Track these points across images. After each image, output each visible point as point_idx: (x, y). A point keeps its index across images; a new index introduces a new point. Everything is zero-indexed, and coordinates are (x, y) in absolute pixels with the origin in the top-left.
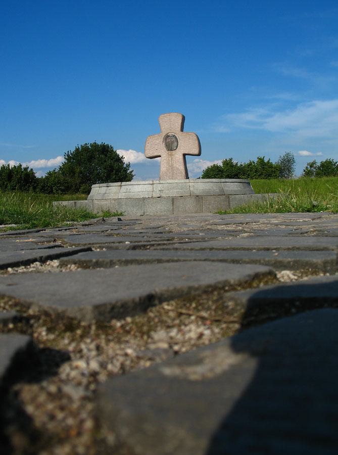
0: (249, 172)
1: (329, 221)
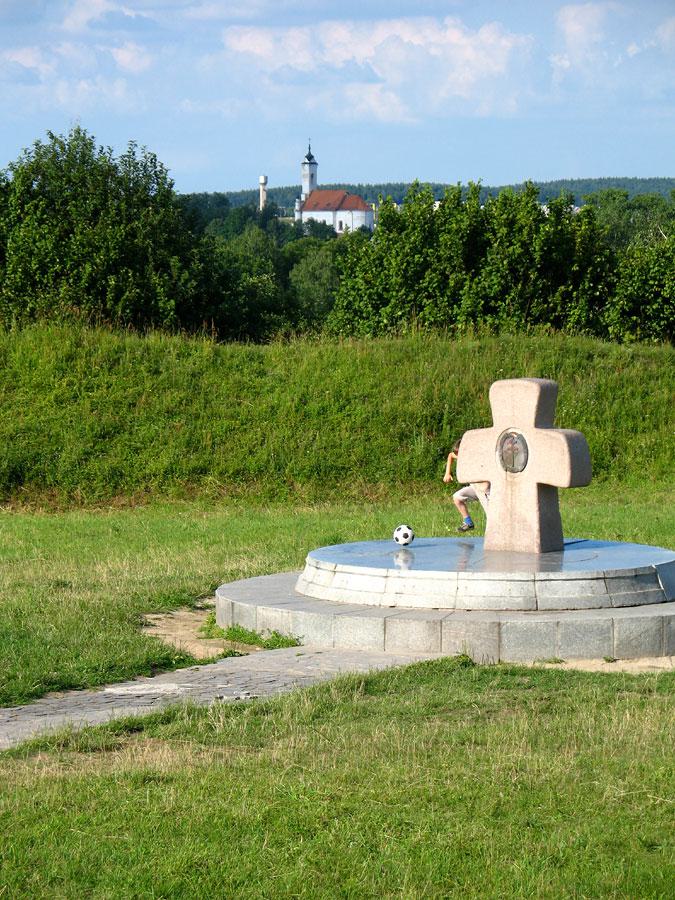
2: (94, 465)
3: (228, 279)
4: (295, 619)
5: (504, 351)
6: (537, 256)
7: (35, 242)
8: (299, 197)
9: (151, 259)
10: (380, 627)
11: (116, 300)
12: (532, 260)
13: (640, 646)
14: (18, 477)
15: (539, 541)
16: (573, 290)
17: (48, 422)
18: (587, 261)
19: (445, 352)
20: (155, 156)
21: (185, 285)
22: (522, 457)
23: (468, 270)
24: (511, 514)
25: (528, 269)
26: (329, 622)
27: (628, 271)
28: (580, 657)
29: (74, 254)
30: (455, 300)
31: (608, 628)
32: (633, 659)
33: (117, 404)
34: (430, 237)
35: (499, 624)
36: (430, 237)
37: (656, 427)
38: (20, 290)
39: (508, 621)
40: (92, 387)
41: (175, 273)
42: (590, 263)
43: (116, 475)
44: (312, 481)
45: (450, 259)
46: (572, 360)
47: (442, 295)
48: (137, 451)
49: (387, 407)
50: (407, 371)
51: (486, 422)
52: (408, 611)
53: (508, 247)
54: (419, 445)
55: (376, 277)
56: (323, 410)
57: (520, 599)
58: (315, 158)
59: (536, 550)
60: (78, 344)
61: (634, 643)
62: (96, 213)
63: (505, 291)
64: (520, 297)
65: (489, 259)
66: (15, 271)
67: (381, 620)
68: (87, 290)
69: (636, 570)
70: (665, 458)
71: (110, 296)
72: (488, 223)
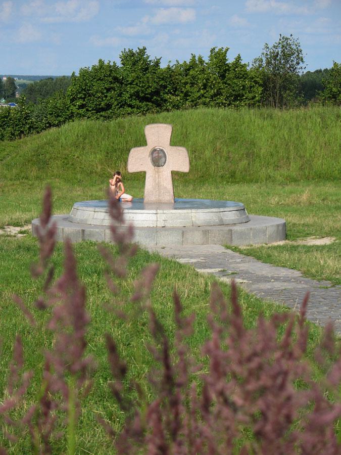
0: (188, 86)
1: (70, 451)
24: (158, 185)
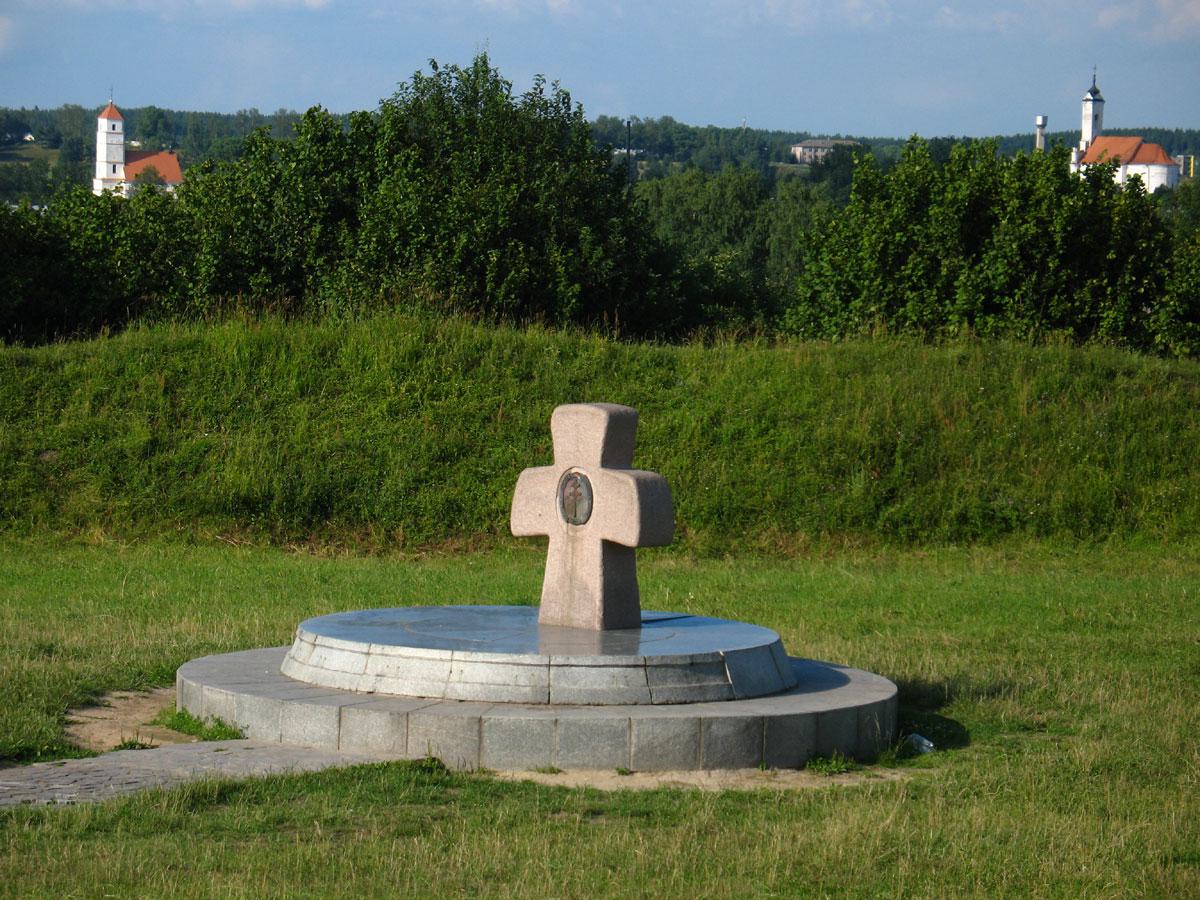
2: (423, 497)
3: (666, 258)
4: (240, 703)
5: (996, 363)
6: (1058, 238)
7: (396, 203)
8: (1078, 146)
9: (553, 229)
10: (335, 718)
11: (498, 282)
12: (1052, 244)
13: (667, 756)
14: (324, 508)
15: (601, 615)
16: (1108, 285)
17: (374, 437)
18: (1127, 247)
19: (913, 363)
20: (567, 94)
21: (597, 265)
22: (585, 505)
23: (967, 254)
24: (570, 577)
25: (1047, 255)
26: (276, 710)
27: (1184, 261)
28: (583, 767)
29: (449, 220)
30: (948, 292)
31: (623, 730)
32: (656, 772)
33: (468, 417)
34: (918, 207)
35: (480, 720)
36: (918, 207)
37: (1186, 471)
38: (375, 265)
39: (493, 717)
40: (440, 395)
41: (586, 247)
42: (1132, 250)
43: (453, 508)
44: (709, 527)
45: (942, 239)
46: (1084, 377)
47: (930, 287)
48: (484, 479)
49: (822, 432)
50: (858, 385)
51: (545, 457)
52: (387, 699)
53: (1021, 225)
54: (857, 485)
55: (846, 259)
56: (739, 435)
57: (528, 688)
58: (1101, 93)
59: (597, 626)
60: (429, 338)
61: (658, 751)
62: (485, 167)
63: (1014, 283)
64: (1036, 291)
65: (995, 240)
66: (368, 242)
67: (335, 709)
68: (461, 268)
69: (692, 657)
70: (1189, 512)
71: (489, 276)
72: (997, 193)
